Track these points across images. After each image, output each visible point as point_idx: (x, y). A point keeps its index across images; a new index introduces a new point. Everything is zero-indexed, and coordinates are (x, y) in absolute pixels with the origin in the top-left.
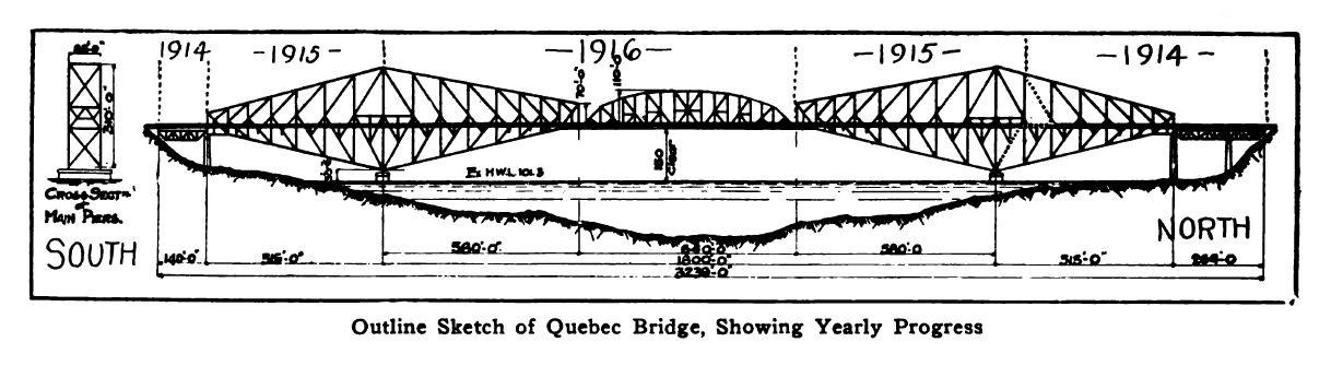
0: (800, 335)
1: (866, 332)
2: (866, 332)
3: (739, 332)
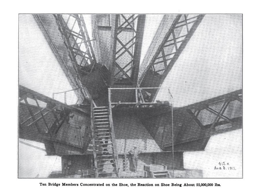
0: (181, 186)
3: (94, 184)
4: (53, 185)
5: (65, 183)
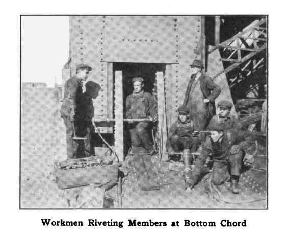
5: (135, 221)
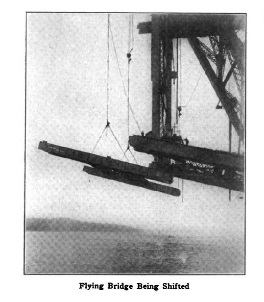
0: (103, 289)
1: (86, 288)
2: (86, 288)
4: (118, 288)
